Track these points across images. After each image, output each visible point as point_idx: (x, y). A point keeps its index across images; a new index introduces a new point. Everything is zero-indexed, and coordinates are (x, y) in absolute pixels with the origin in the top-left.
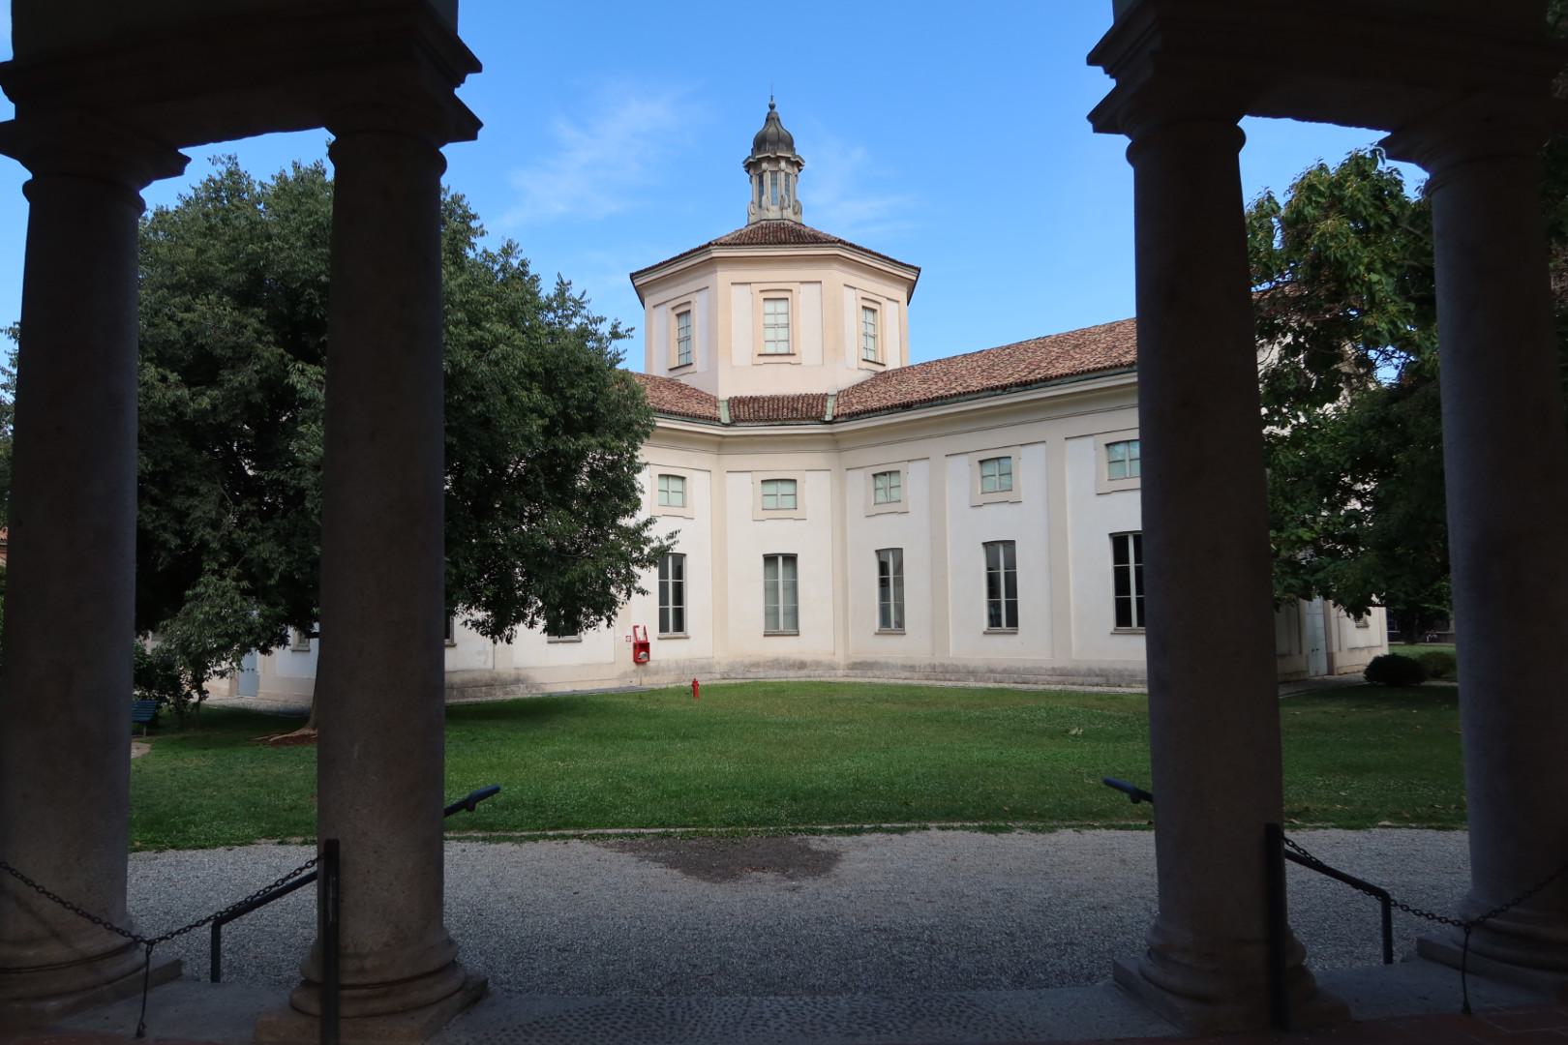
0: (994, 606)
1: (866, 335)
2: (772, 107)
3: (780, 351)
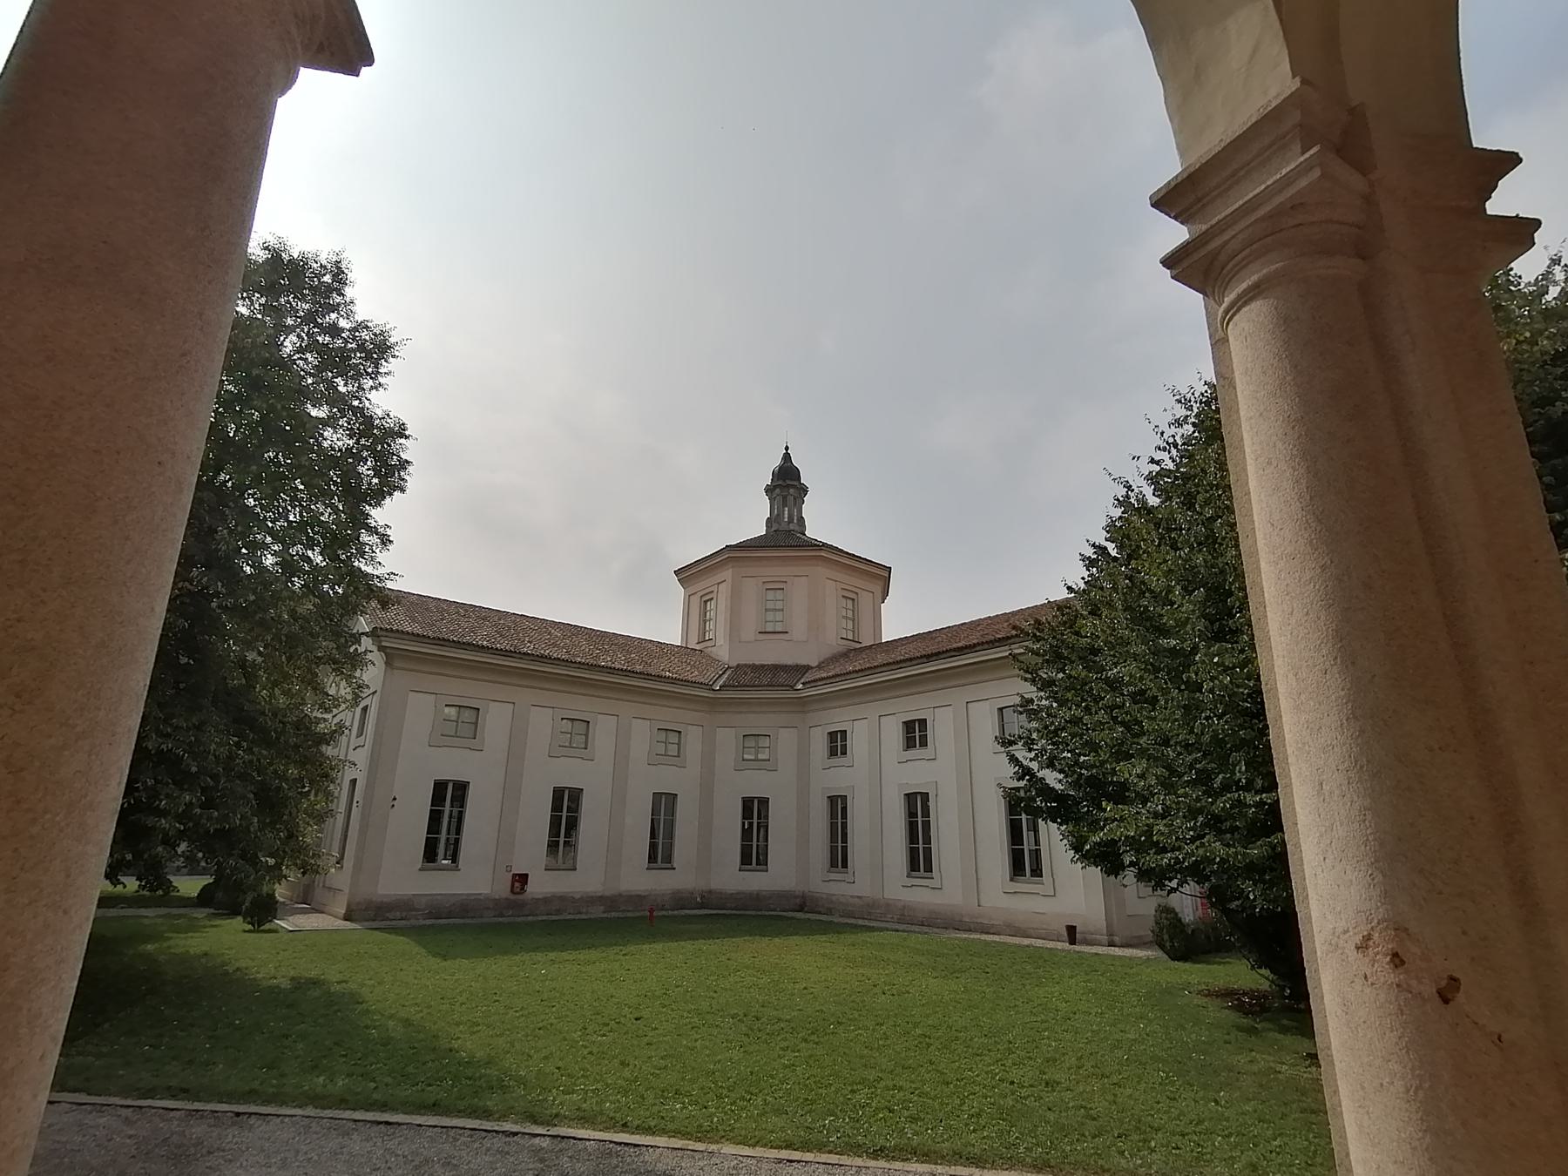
0: (653, 847)
1: (846, 618)
2: (787, 448)
3: (767, 630)
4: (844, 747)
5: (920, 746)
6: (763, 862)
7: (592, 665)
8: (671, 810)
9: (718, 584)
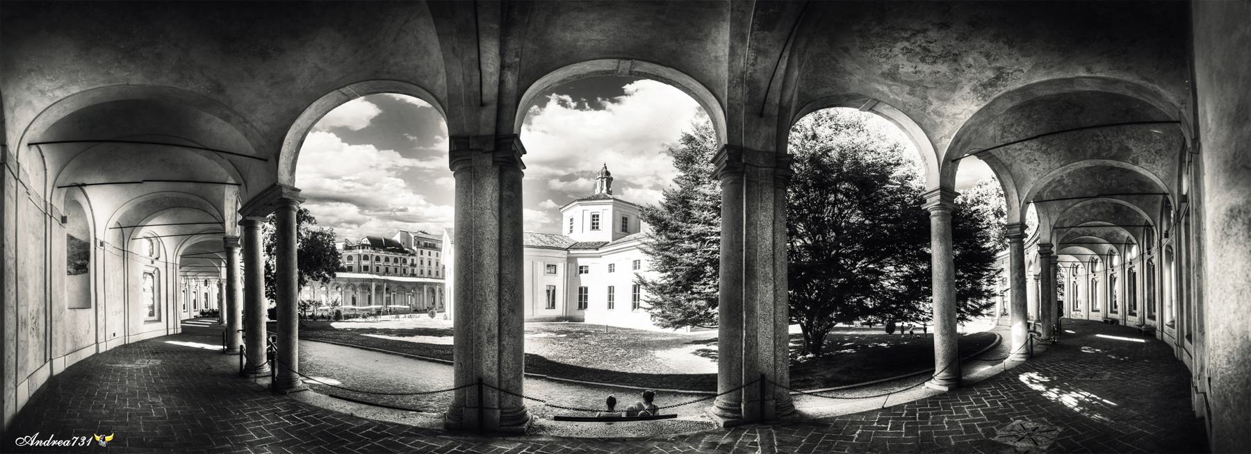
4: (639, 266)
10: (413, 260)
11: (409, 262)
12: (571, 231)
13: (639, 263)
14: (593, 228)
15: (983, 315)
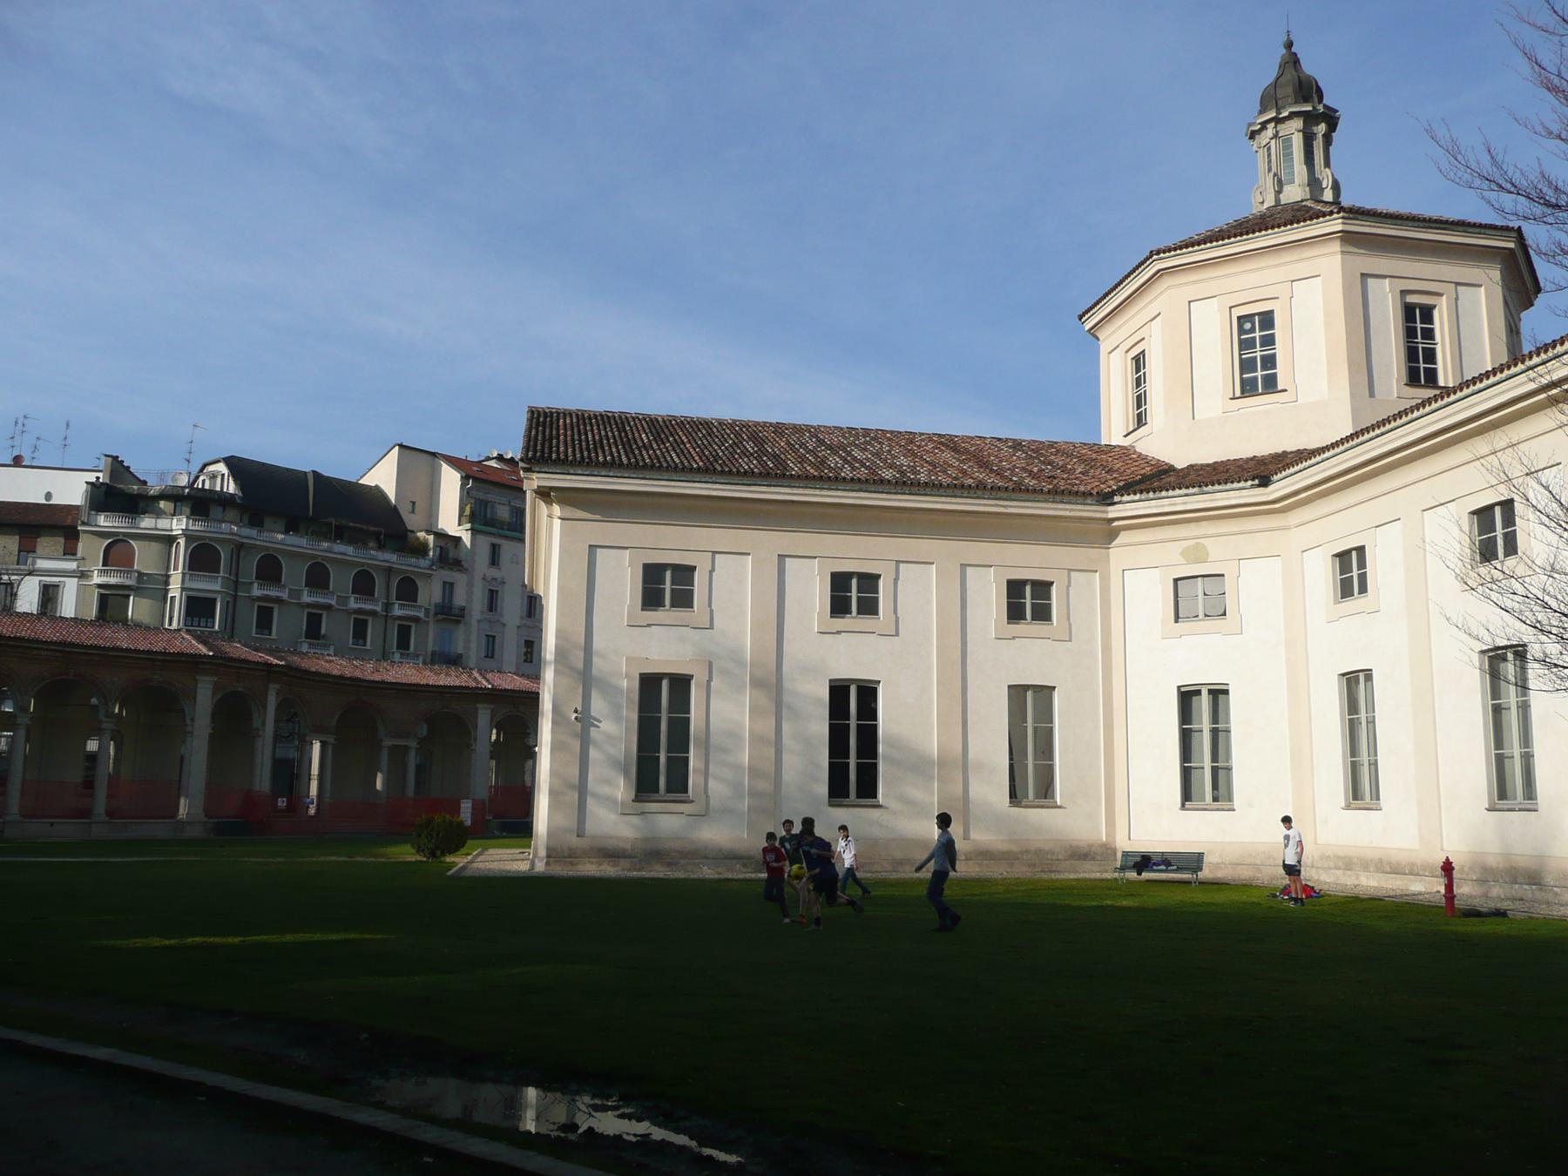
2: (1289, 45)
4: (1363, 579)
5: (859, 613)
6: (1221, 792)
7: (852, 479)
8: (1045, 713)
9: (1292, 281)
10: (449, 587)
11: (430, 594)
12: (1140, 421)
13: (1362, 564)
14: (1248, 389)
15: (493, 685)
